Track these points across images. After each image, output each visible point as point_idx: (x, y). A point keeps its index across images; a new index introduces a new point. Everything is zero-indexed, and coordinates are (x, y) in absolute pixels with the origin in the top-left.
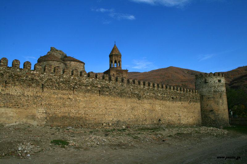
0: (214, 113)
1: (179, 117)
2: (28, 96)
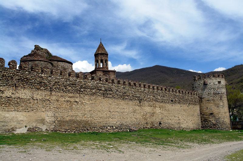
0: (215, 117)
1: (178, 120)
2: (37, 99)
